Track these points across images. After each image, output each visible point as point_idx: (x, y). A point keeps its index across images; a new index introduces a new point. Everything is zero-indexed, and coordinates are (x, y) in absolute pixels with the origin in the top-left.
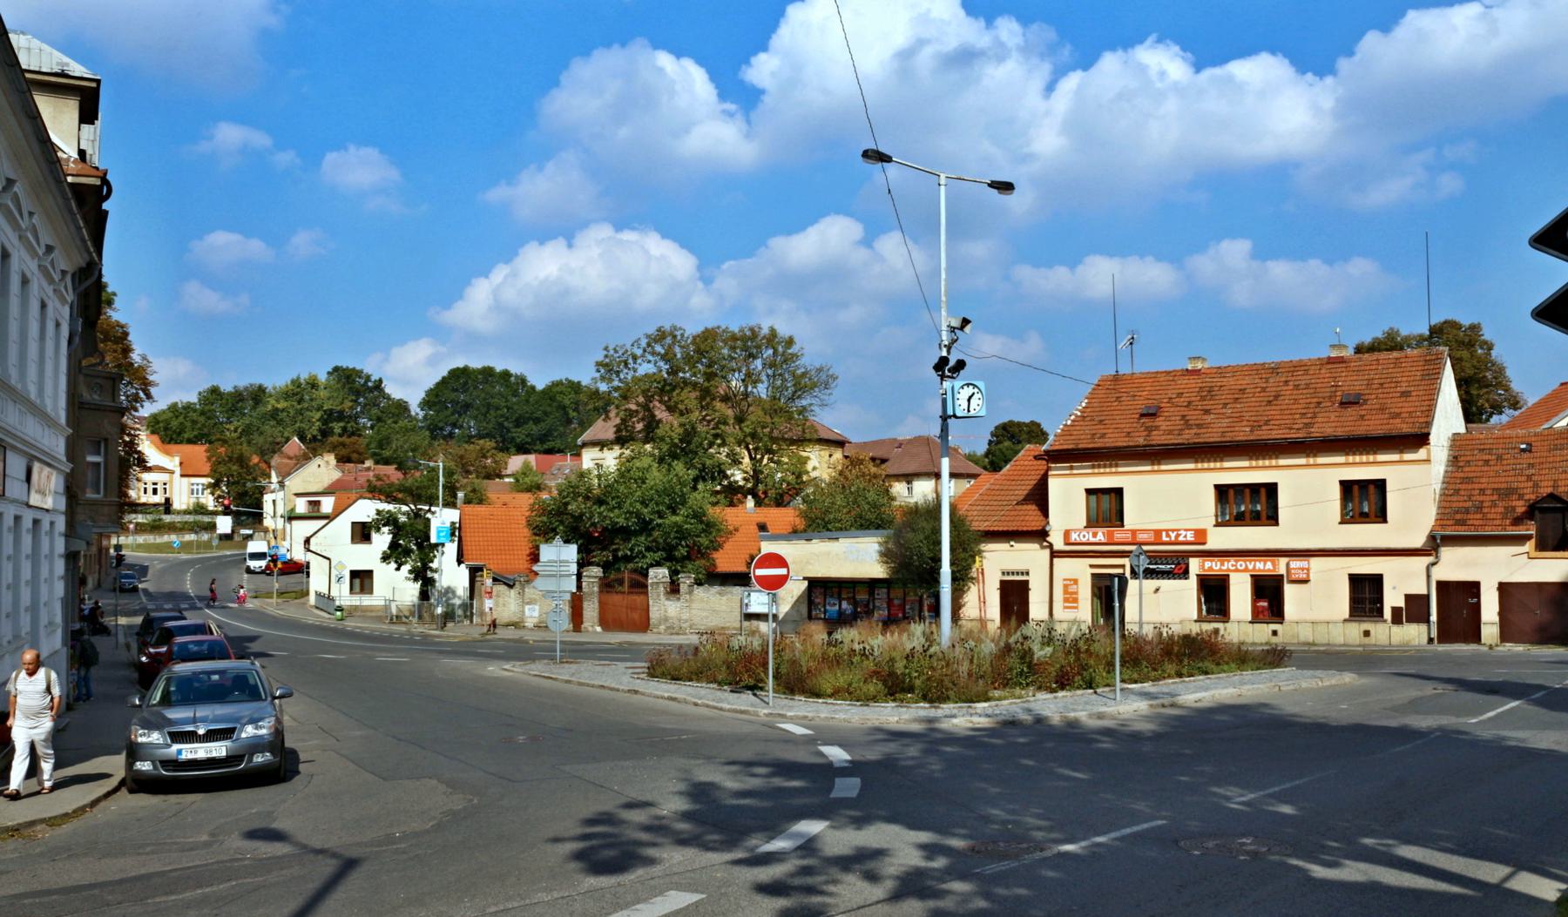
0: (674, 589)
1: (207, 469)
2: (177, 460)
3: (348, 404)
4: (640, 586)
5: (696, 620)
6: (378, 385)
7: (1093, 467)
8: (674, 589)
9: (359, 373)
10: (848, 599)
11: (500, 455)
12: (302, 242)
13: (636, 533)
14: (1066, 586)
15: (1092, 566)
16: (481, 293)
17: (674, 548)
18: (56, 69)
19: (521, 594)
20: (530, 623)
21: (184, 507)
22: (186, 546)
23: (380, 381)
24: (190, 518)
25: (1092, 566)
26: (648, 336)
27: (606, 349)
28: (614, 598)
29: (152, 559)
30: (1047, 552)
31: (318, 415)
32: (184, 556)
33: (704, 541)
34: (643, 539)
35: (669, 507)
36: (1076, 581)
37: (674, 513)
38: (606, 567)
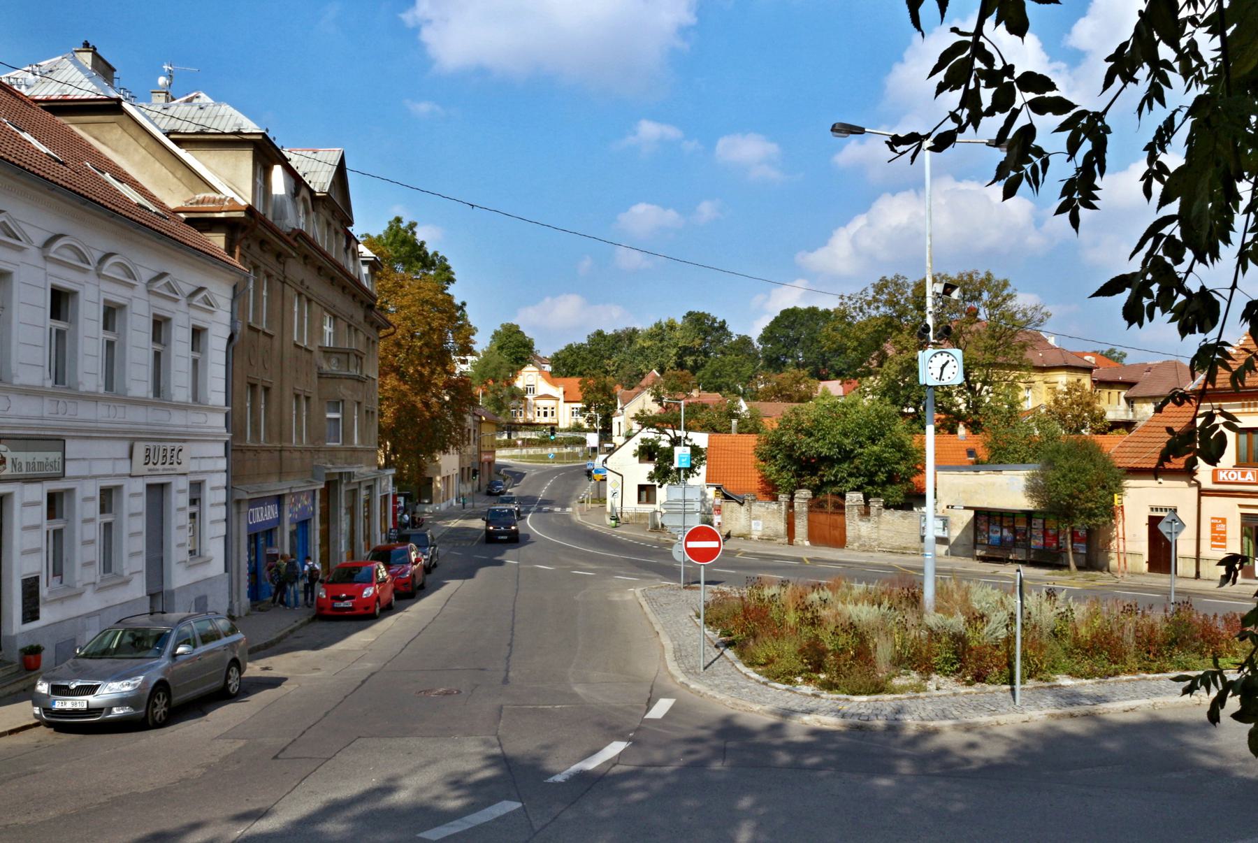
0: (866, 513)
1: (579, 396)
2: (561, 390)
3: (697, 341)
4: (840, 508)
5: (883, 540)
6: (723, 326)
7: (1243, 406)
8: (866, 513)
9: (706, 316)
10: (1008, 527)
11: (812, 382)
12: (706, 209)
13: (839, 461)
14: (1213, 525)
15: (1240, 506)
16: (842, 242)
17: (876, 473)
18: (235, 130)
19: (749, 510)
20: (755, 536)
21: (567, 426)
22: (559, 457)
23: (724, 322)
24: (568, 434)
25: (1240, 506)
26: (874, 286)
27: (841, 297)
28: (822, 518)
29: (530, 468)
30: (1195, 490)
31: (674, 351)
32: (556, 466)
33: (902, 467)
34: (846, 465)
35: (869, 438)
36: (1224, 521)
37: (873, 443)
38: (816, 490)
